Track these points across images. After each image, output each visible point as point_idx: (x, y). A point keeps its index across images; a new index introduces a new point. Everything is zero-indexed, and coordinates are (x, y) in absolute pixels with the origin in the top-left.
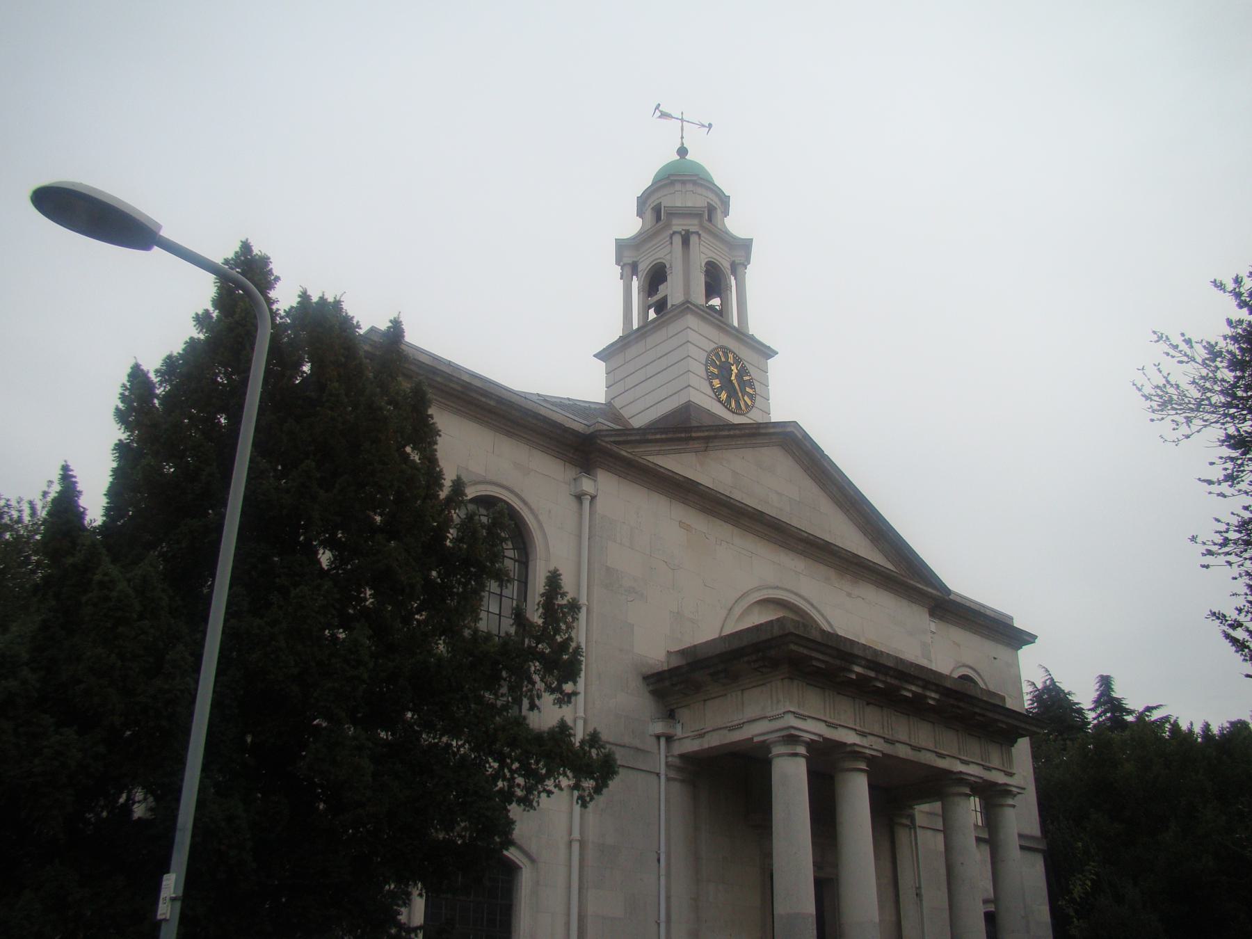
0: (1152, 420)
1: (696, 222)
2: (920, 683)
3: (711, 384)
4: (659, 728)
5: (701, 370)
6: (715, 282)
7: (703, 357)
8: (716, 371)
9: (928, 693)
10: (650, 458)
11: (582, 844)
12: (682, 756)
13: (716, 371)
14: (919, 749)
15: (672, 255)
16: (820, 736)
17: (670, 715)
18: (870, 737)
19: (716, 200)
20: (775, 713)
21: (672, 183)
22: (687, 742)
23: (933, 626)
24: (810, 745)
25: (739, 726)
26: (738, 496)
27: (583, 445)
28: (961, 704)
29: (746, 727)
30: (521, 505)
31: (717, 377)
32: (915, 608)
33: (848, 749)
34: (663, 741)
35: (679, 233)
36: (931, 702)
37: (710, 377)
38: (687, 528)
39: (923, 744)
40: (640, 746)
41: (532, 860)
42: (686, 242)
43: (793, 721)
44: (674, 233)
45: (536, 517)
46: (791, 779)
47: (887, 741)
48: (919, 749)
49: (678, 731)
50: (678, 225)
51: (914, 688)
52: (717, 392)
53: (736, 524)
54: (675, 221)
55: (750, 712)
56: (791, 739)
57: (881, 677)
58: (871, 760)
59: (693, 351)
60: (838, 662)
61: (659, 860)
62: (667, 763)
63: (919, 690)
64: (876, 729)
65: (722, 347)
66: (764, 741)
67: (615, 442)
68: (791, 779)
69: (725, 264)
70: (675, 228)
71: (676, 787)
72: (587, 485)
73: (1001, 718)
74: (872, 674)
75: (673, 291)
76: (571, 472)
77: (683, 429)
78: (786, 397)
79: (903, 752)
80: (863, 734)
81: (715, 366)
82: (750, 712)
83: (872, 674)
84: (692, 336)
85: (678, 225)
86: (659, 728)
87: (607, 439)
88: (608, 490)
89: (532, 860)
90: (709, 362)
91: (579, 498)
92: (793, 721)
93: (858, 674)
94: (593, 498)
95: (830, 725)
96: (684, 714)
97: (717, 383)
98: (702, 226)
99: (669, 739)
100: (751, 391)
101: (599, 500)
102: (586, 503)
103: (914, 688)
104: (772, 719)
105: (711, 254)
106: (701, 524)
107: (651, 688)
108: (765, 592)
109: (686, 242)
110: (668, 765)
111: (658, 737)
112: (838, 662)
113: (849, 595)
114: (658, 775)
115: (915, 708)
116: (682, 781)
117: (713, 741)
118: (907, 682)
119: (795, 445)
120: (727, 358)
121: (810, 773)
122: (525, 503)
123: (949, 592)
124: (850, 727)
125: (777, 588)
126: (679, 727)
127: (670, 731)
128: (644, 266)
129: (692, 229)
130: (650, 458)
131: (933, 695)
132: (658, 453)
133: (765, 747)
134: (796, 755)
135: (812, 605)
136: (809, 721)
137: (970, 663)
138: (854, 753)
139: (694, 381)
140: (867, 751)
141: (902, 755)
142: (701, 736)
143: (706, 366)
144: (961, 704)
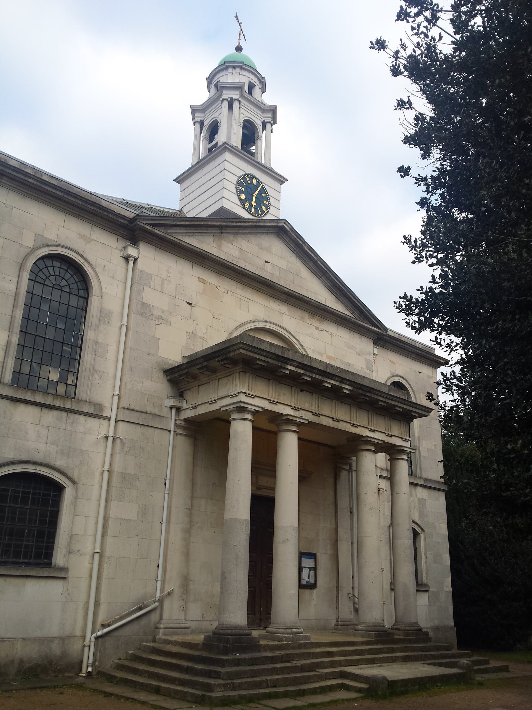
0: (404, 171)
1: (238, 92)
2: (337, 378)
3: (239, 198)
4: (172, 402)
5: (233, 188)
6: (250, 135)
7: (235, 180)
8: (243, 189)
9: (344, 386)
10: (180, 237)
11: (110, 472)
12: (186, 420)
13: (243, 189)
14: (338, 421)
15: (222, 113)
16: (262, 408)
17: (181, 395)
18: (301, 411)
19: (256, 80)
20: (233, 393)
21: (227, 68)
22: (188, 411)
23: (376, 351)
24: (255, 413)
25: (215, 402)
26: (242, 264)
27: (137, 228)
28: (368, 394)
29: (218, 402)
30: (83, 261)
31: (243, 192)
32: (364, 339)
33: (284, 418)
34: (174, 411)
35: (226, 100)
36: (346, 391)
37: (239, 192)
38: (204, 282)
39: (342, 418)
40: (157, 413)
41: (74, 482)
42: (231, 107)
43: (243, 398)
44: (224, 100)
45: (94, 269)
46: (242, 432)
47: (314, 414)
48: (338, 421)
49: (185, 405)
50: (227, 94)
51: (333, 382)
52: (243, 202)
53: (240, 282)
54: (224, 92)
55: (222, 392)
56: (242, 409)
57: (308, 373)
58: (299, 425)
59: (228, 175)
60: (276, 363)
61: (165, 484)
62: (175, 424)
63: (337, 384)
64: (307, 406)
65: (248, 175)
66: (227, 410)
67: (149, 224)
68: (242, 432)
69: (259, 123)
70: (224, 97)
71: (181, 440)
72: (132, 251)
73: (398, 404)
74: (302, 372)
75: (221, 138)
76: (122, 243)
77: (222, 224)
78: (286, 206)
79: (326, 421)
80: (296, 409)
81: (242, 186)
82: (222, 393)
83: (302, 372)
84: (227, 165)
85: (227, 94)
86: (172, 402)
87: (144, 222)
88: (147, 256)
89: (74, 482)
90: (239, 183)
91: (127, 259)
92: (243, 398)
93: (291, 371)
94: (136, 259)
95: (271, 402)
96: (188, 395)
97: (243, 197)
98: (242, 96)
99: (178, 410)
100: (267, 203)
101: (139, 261)
102: (131, 262)
103: (333, 382)
104: (233, 397)
105: (248, 115)
106: (211, 278)
107: (168, 378)
108: (256, 324)
109: (231, 107)
110: (176, 425)
111: (171, 408)
112: (276, 363)
113: (317, 328)
114: (169, 431)
115: (335, 395)
116: (186, 436)
117: (202, 410)
118: (328, 377)
119: (284, 232)
120: (251, 181)
121: (254, 428)
122: (86, 260)
123: (386, 330)
124: (286, 404)
125: (265, 321)
126: (185, 402)
127: (179, 405)
128: (207, 124)
129: (235, 97)
130: (180, 237)
131: (347, 387)
132: (186, 234)
133: (228, 413)
134: (244, 419)
135: (290, 333)
136: (256, 398)
137: (401, 375)
138: (289, 421)
139: (226, 194)
140: (297, 419)
141: (324, 423)
142: (195, 407)
143: (236, 185)
144: (368, 394)
